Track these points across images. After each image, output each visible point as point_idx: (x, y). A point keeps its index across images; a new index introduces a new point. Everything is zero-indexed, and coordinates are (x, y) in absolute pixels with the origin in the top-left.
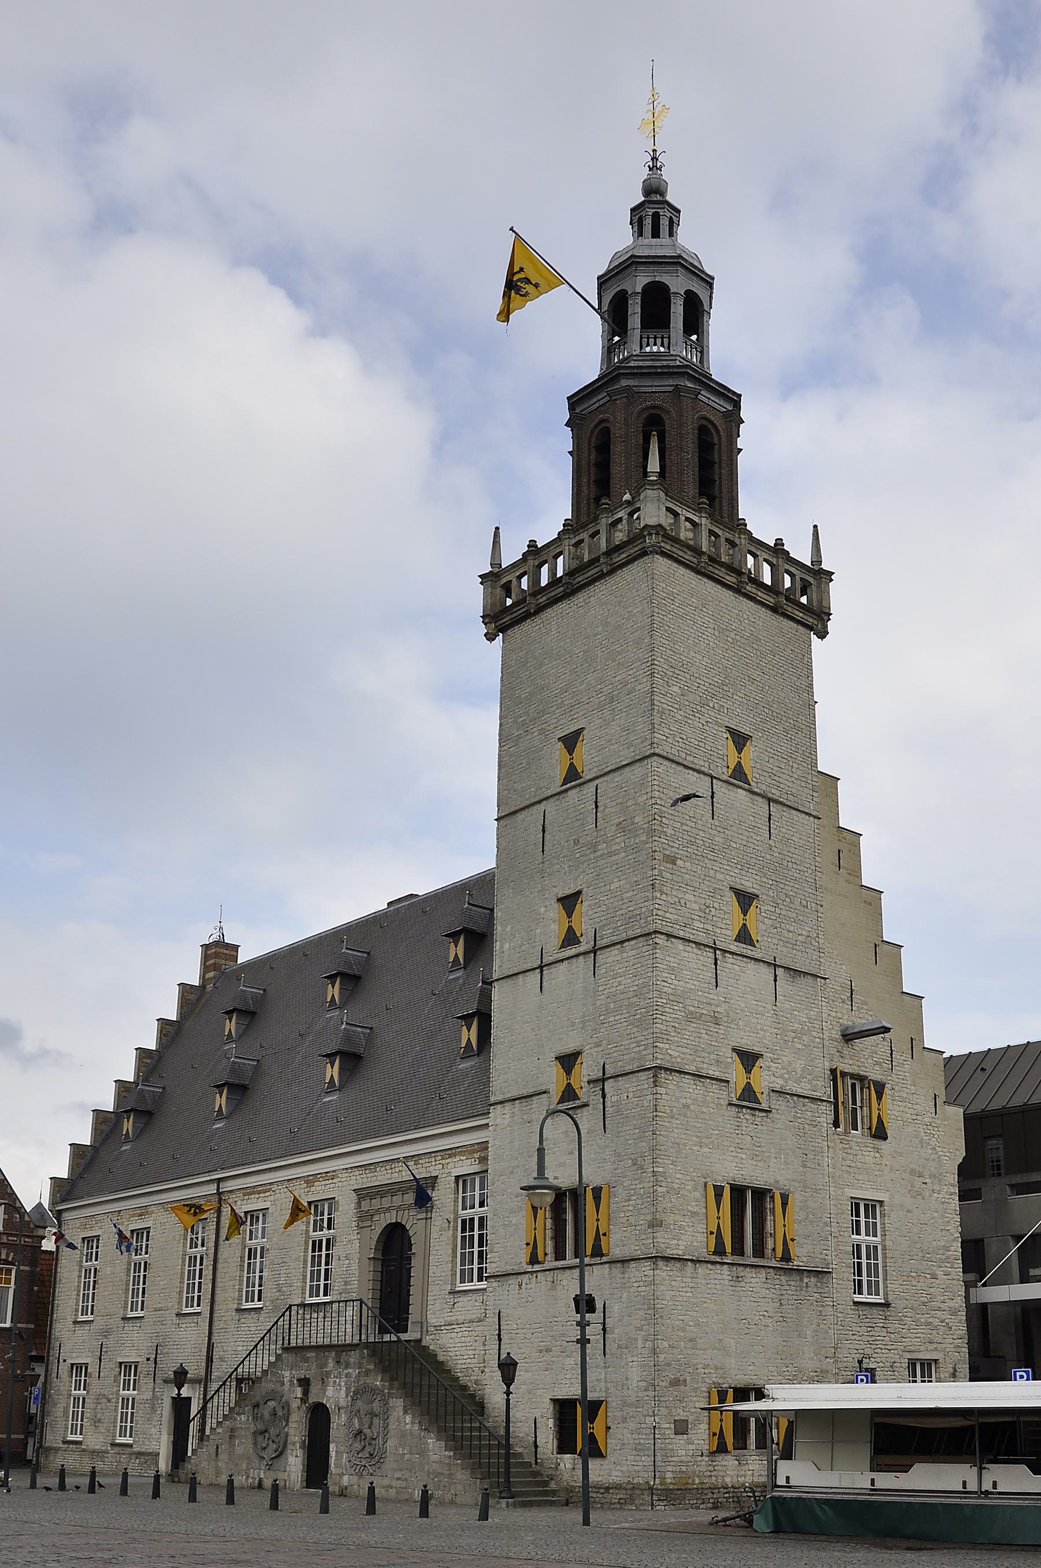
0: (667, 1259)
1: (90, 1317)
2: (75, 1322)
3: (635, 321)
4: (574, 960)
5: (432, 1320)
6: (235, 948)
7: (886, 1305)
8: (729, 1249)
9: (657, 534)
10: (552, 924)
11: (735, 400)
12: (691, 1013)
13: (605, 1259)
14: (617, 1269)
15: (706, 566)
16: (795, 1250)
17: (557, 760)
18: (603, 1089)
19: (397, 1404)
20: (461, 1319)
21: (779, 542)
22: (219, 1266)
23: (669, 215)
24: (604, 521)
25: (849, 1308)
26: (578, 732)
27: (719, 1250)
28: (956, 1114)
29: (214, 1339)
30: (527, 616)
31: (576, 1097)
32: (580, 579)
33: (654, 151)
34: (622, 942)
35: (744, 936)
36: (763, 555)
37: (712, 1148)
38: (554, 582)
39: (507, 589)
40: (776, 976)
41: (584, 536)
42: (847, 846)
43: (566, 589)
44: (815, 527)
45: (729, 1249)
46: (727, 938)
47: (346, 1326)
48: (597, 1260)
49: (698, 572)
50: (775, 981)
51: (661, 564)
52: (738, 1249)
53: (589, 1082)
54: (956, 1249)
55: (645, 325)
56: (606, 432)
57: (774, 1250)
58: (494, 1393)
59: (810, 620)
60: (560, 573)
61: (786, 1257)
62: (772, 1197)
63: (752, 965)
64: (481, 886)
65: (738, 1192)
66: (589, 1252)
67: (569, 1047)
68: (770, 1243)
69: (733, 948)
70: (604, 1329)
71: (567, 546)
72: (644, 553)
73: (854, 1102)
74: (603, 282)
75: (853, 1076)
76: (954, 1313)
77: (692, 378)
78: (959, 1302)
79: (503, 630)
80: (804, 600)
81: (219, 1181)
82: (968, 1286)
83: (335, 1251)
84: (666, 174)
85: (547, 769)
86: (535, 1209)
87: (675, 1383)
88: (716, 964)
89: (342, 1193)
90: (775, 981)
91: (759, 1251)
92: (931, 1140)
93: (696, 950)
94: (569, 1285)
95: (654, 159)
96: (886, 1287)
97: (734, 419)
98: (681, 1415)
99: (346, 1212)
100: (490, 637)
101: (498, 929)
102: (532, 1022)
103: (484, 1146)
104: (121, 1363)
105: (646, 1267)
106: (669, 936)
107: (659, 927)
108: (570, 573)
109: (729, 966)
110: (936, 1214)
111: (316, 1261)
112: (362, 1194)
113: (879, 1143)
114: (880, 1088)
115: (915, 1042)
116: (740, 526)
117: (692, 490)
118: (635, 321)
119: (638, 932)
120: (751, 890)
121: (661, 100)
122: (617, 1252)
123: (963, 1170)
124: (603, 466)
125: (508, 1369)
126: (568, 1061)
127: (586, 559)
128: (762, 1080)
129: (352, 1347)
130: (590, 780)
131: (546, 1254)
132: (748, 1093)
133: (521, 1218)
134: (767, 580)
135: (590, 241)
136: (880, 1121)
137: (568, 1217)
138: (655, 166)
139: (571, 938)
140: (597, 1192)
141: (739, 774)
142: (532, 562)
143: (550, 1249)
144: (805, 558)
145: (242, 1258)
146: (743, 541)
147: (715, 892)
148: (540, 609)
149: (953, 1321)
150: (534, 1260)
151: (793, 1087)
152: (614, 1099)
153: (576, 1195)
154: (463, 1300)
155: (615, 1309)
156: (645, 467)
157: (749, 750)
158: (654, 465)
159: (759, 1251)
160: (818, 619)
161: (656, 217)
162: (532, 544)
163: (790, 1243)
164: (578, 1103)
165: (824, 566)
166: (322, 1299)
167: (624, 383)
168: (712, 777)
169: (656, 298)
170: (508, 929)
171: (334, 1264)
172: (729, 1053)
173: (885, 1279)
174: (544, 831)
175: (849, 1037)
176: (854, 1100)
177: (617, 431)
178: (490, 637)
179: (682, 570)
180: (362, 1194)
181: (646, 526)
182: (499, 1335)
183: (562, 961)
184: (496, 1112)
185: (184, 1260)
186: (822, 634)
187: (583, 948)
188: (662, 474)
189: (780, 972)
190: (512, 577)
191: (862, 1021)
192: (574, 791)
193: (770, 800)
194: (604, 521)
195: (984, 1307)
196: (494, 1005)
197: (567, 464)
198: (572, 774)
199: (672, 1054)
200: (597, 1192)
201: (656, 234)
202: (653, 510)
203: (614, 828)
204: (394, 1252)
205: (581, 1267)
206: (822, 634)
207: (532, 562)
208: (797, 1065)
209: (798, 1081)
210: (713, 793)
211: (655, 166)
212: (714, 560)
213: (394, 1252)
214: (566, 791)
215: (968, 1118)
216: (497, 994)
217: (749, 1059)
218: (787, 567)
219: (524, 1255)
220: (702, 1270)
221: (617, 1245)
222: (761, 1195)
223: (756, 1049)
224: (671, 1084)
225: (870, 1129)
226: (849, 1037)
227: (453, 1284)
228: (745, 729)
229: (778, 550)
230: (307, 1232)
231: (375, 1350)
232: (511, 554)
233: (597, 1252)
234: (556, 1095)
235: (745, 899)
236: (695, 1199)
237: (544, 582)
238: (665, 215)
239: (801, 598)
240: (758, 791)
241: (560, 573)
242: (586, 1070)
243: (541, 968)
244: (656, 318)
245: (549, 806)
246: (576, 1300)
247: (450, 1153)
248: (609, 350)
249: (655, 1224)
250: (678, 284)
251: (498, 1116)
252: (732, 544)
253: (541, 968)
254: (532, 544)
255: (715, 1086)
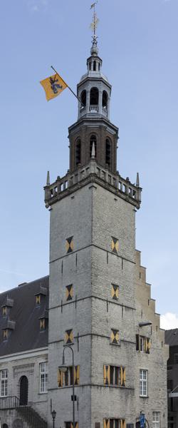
0: (94, 385)
3: (88, 101)
7: (148, 397)
10: (65, 293)
11: (116, 131)
15: (108, 186)
17: (66, 246)
21: (128, 178)
25: (139, 398)
26: (71, 330)
27: (107, 383)
28: (167, 346)
30: (57, 200)
32: (72, 190)
35: (115, 298)
36: (123, 183)
37: (105, 355)
38: (65, 190)
41: (73, 175)
43: (68, 193)
47: (13, 402)
49: (106, 189)
52: (111, 382)
54: (166, 383)
55: (91, 104)
56: (80, 141)
58: (50, 420)
59: (135, 204)
60: (66, 187)
61: (123, 385)
63: (116, 306)
64: (45, 282)
67: (69, 328)
68: (119, 381)
71: (69, 179)
74: (79, 87)
76: (164, 399)
77: (106, 123)
78: (166, 397)
79: (50, 205)
80: (133, 197)
82: (168, 392)
83: (8, 383)
85: (65, 247)
86: (60, 372)
89: (10, 367)
91: (116, 383)
92: (160, 352)
94: (69, 392)
97: (116, 137)
99: (10, 373)
101: (50, 295)
102: (59, 321)
103: (47, 355)
105: (89, 387)
106: (96, 298)
107: (93, 294)
108: (69, 188)
109: (111, 305)
111: (3, 386)
112: (15, 368)
114: (148, 339)
115: (158, 327)
116: (117, 174)
117: (104, 161)
118: (88, 101)
121: (97, 17)
123: (169, 362)
124: (79, 158)
125: (54, 413)
126: (69, 332)
129: (12, 409)
133: (57, 374)
134: (124, 191)
135: (74, 74)
137: (69, 375)
139: (70, 298)
140: (76, 367)
142: (59, 183)
146: (118, 179)
147: (107, 285)
149: (164, 402)
150: (60, 385)
151: (126, 339)
153: (71, 368)
154: (42, 396)
155: (80, 399)
156: (91, 153)
157: (117, 243)
158: (93, 154)
159: (116, 383)
160: (137, 203)
161: (95, 62)
162: (58, 177)
165: (140, 186)
166: (5, 396)
167: (85, 124)
169: (95, 92)
171: (8, 387)
172: (110, 330)
175: (141, 325)
176: (140, 343)
177: (83, 140)
180: (15, 368)
184: (50, 346)
187: (73, 300)
188: (95, 156)
190: (53, 188)
191: (144, 321)
193: (123, 258)
194: (80, 171)
195: (172, 398)
196: (50, 316)
197: (68, 150)
198: (70, 250)
199: (95, 330)
200: (76, 367)
201: (95, 69)
202: (93, 169)
204: (24, 382)
205: (73, 387)
207: (59, 183)
208: (128, 334)
209: (128, 372)
212: (110, 185)
213: (24, 382)
215: (170, 347)
216: (50, 313)
217: (115, 331)
219: (57, 384)
220: (103, 388)
221: (80, 382)
222: (118, 368)
223: (117, 329)
224: (95, 339)
226: (141, 325)
228: (116, 237)
229: (127, 181)
231: (18, 409)
232: (53, 181)
233: (76, 383)
234: (66, 342)
235: (116, 287)
236: (100, 370)
237: (62, 190)
238: (98, 61)
241: (66, 187)
242: (74, 334)
244: (94, 101)
245: (64, 259)
246: (72, 397)
247: (38, 356)
248: (81, 111)
249: (91, 376)
250: (101, 88)
251: (51, 347)
252: (114, 179)
254: (58, 177)
255: (106, 339)
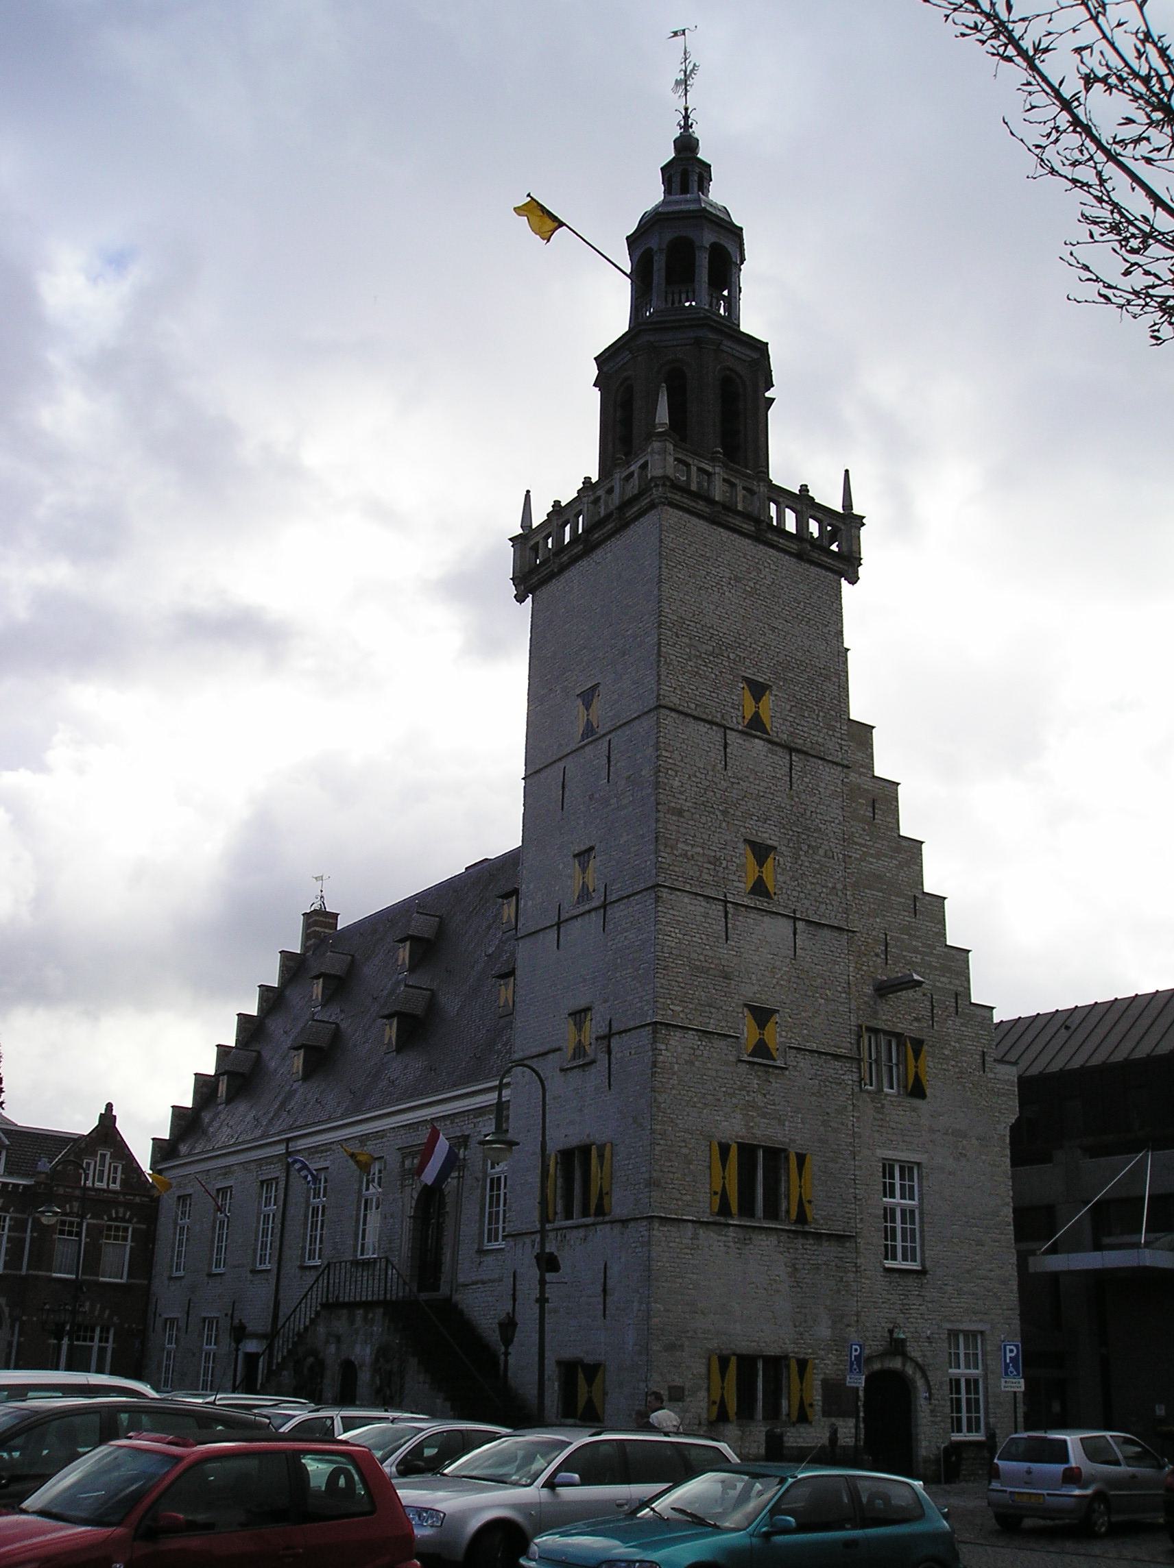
1: (182, 1273)
2: (170, 1278)
4: (587, 916)
5: (462, 1279)
6: (335, 916)
7: (923, 1272)
8: (734, 1207)
9: (664, 485)
12: (697, 968)
13: (607, 1218)
14: (617, 1228)
15: (720, 515)
16: (810, 1212)
18: (609, 1046)
19: (413, 1362)
20: (485, 1278)
21: (804, 488)
22: (287, 1223)
23: (698, 170)
24: (617, 476)
27: (724, 1210)
29: (281, 1295)
31: (585, 1054)
33: (686, 109)
34: (628, 897)
35: (759, 888)
37: (716, 1107)
38: (575, 537)
39: (535, 548)
40: (795, 929)
42: (884, 797)
43: (586, 545)
44: (847, 471)
45: (734, 1207)
46: (740, 888)
48: (600, 1219)
50: (795, 934)
51: (672, 516)
52: (747, 1209)
53: (597, 1039)
57: (788, 1212)
61: (802, 1218)
62: (787, 1158)
65: (747, 1151)
66: (592, 1211)
69: (747, 902)
70: (605, 1291)
72: (652, 506)
73: (890, 1060)
74: (632, 241)
75: (886, 1033)
77: (714, 329)
78: (1011, 1272)
80: (834, 547)
81: (288, 1140)
84: (697, 131)
87: (671, 1348)
88: (726, 917)
90: (795, 934)
91: (772, 1211)
93: (703, 904)
95: (686, 117)
96: (923, 1252)
98: (678, 1382)
100: (520, 598)
104: (204, 1319)
110: (982, 1178)
113: (917, 1102)
119: (642, 886)
120: (770, 842)
122: (618, 1211)
124: (627, 422)
126: (579, 1015)
127: (602, 514)
128: (775, 1036)
130: (604, 735)
131: (556, 1213)
132: (762, 1049)
136: (917, 1079)
138: (686, 126)
140: (601, 1148)
141: (756, 725)
143: (559, 1208)
144: (837, 506)
145: (306, 1217)
146: (763, 489)
148: (563, 569)
152: (619, 1055)
154: (489, 1259)
157: (768, 700)
159: (772, 1211)
160: (849, 565)
162: (557, 503)
163: (807, 1205)
164: (587, 1060)
165: (855, 511)
168: (726, 728)
170: (532, 886)
173: (922, 1245)
174: (563, 788)
175: (884, 990)
178: (520, 598)
179: (695, 520)
181: (653, 478)
182: (514, 1295)
183: (576, 917)
185: (259, 1219)
186: (853, 580)
189: (800, 925)
190: (539, 538)
192: (591, 747)
198: (589, 730)
203: (623, 782)
206: (853, 580)
210: (726, 743)
211: (686, 126)
214: (582, 747)
217: (762, 1015)
218: (812, 513)
221: (620, 1204)
222: (775, 1155)
225: (906, 1087)
226: (884, 990)
227: (481, 1242)
230: (360, 1190)
232: (538, 518)
233: (600, 1211)
235: (761, 852)
239: (833, 545)
240: (777, 740)
243: (558, 924)
245: (569, 763)
246: (538, 1257)
253: (558, 924)
254: (557, 503)
